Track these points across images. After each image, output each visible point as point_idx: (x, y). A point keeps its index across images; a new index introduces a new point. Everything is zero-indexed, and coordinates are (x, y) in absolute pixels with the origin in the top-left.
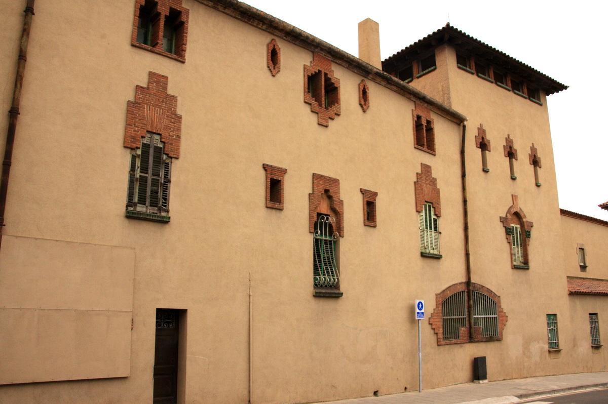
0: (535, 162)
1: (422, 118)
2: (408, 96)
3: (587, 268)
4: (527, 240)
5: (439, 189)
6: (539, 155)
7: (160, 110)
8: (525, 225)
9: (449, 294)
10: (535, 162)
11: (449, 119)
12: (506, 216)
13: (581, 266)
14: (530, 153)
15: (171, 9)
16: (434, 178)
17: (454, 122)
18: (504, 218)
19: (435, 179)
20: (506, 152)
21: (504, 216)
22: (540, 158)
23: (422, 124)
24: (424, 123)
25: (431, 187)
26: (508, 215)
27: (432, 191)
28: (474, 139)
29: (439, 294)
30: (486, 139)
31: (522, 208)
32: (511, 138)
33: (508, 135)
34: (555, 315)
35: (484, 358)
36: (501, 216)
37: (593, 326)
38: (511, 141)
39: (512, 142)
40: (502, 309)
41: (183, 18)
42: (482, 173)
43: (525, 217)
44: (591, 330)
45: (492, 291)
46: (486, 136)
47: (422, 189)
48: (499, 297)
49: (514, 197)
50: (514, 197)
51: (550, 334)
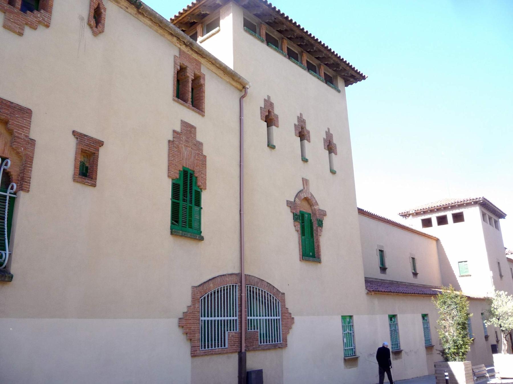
0: (330, 147)
1: (188, 69)
2: (170, 37)
3: (387, 271)
4: (319, 230)
5: (205, 157)
6: (335, 141)
7: (193, 151)
8: (317, 213)
9: (213, 287)
10: (330, 147)
12: (295, 201)
13: (413, 273)
14: (325, 137)
15: (195, 74)
16: (198, 142)
17: (233, 86)
18: (291, 202)
19: (201, 144)
20: (297, 132)
21: (293, 200)
22: (335, 145)
23: (188, 77)
24: (191, 76)
25: (193, 151)
26: (297, 199)
27: (195, 157)
28: (260, 109)
29: (196, 287)
30: (274, 112)
31: (313, 194)
32: (304, 117)
33: (301, 114)
34: (351, 317)
35: (262, 370)
36: (288, 199)
37: (425, 326)
38: (304, 122)
39: (305, 122)
40: (287, 309)
41: (202, 81)
42: (267, 149)
43: (317, 204)
44: (391, 333)
45: (274, 287)
46: (273, 110)
47: (179, 151)
48: (284, 294)
49: (305, 182)
50: (305, 182)
51: (345, 340)
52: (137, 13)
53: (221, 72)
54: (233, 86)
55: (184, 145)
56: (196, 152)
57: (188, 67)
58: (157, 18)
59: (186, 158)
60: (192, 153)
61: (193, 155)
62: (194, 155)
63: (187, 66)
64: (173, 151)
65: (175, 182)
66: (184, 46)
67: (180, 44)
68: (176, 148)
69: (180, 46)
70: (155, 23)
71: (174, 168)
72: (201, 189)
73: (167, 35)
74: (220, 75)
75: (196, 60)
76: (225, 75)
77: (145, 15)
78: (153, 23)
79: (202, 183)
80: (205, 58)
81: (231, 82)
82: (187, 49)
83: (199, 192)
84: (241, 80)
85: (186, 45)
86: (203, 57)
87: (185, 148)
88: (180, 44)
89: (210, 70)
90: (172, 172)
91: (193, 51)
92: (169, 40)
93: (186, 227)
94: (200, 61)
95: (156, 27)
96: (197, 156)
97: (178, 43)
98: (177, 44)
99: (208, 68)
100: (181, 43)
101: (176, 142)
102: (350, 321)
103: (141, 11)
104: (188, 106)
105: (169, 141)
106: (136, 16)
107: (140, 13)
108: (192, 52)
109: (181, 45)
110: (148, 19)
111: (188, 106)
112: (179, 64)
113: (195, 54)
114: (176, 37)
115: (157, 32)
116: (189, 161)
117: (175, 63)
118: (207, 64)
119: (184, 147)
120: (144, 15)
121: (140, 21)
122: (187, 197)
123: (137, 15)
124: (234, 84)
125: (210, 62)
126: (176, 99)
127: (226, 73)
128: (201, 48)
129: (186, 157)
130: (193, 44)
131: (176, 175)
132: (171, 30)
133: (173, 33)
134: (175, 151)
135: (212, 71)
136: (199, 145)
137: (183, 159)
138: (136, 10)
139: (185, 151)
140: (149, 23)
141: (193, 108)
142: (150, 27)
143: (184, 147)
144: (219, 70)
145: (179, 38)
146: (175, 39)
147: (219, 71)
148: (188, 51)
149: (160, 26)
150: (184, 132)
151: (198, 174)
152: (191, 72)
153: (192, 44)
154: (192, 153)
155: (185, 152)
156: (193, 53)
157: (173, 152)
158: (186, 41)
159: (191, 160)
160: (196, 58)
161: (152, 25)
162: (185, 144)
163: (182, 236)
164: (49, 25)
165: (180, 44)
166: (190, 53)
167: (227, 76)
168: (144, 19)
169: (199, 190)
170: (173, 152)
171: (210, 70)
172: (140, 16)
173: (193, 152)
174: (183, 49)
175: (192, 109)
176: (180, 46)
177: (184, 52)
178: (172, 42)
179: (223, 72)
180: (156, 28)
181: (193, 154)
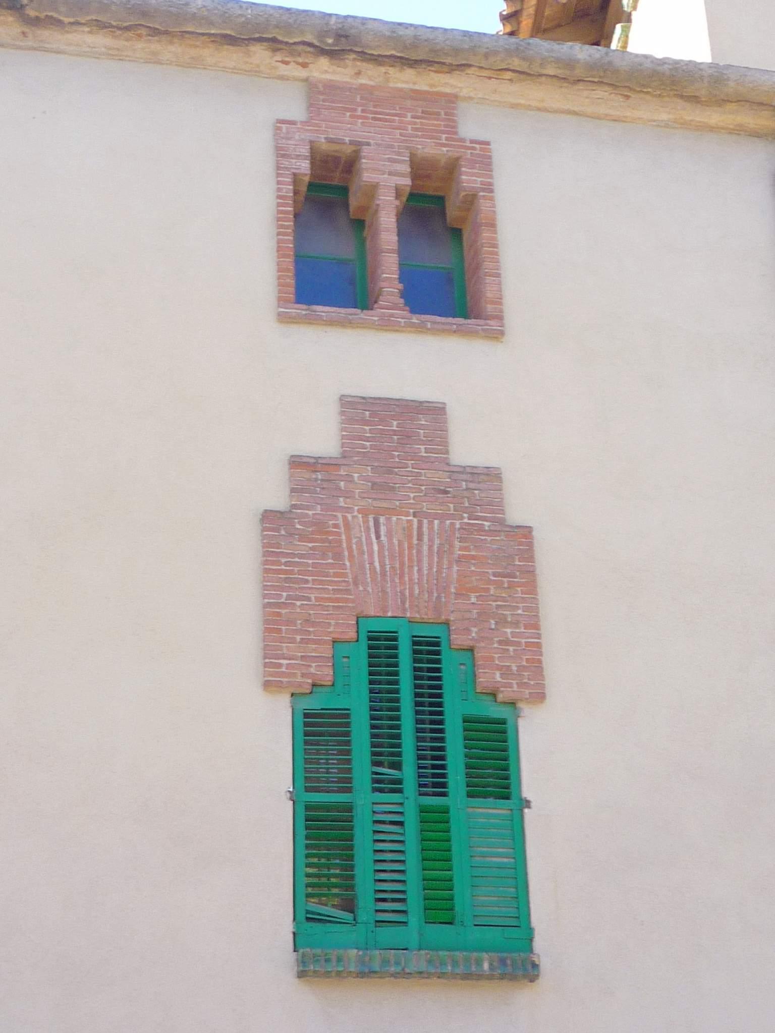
2: (231, 57)
7: (431, 523)
11: (664, 116)
17: (712, 129)
52: (26, 30)
53: (601, 93)
54: (712, 129)
55: (359, 511)
56: (452, 524)
57: (368, 144)
58: (113, 8)
59: (383, 573)
60: (420, 538)
61: (430, 547)
62: (437, 542)
63: (360, 144)
64: (283, 560)
65: (315, 704)
66: (324, 62)
67: (300, 60)
68: (303, 538)
69: (302, 73)
70: (127, 29)
71: (298, 638)
72: (513, 704)
73: (209, 53)
74: (602, 110)
75: (417, 95)
76: (628, 97)
77: (66, 20)
78: (119, 32)
79: (506, 672)
80: (470, 66)
81: (689, 118)
82: (346, 67)
83: (503, 722)
84: (732, 84)
85: (333, 54)
86: (453, 68)
87: (371, 524)
88: (298, 63)
89: (529, 108)
90: (285, 662)
91: (381, 64)
92: (235, 70)
93: (405, 923)
94: (448, 90)
95: (140, 45)
96: (457, 544)
97: (287, 63)
98: (283, 70)
99: (514, 106)
100: (299, 55)
101: (308, 508)
102: (499, 668)
103: (37, 14)
104: (382, 317)
105: (269, 518)
106: (30, 43)
107: (36, 22)
108: (383, 69)
109: (304, 65)
110: (87, 29)
111: (382, 317)
112: (305, 151)
113: (402, 70)
114: (260, 40)
115: (159, 63)
116: (402, 582)
117: (281, 153)
118: (495, 91)
119: (366, 522)
120: (56, 23)
121: (58, 52)
122: (397, 766)
123: (30, 36)
124: (714, 117)
125: (508, 75)
126: (301, 310)
127: (630, 89)
128: (410, 32)
129: (383, 566)
130: (353, 31)
131: (312, 670)
132: (211, 24)
133: (229, 32)
134: (301, 556)
135: (545, 110)
136: (472, 485)
137: (356, 583)
138: (11, 19)
139: (368, 538)
140: (101, 40)
141: (415, 319)
142: (115, 55)
143: (366, 522)
144: (581, 86)
145: (274, 40)
146: (260, 54)
147: (586, 93)
148: (358, 73)
149: (155, 32)
150: (364, 447)
151: (474, 630)
152: (390, 160)
153: (346, 37)
154: (420, 538)
155: (370, 544)
156: (391, 70)
157: (286, 564)
158: (309, 38)
159: (420, 570)
160: (417, 87)
161: (122, 43)
162: (363, 503)
163: (366, 973)
164: (504, 518)
165: (300, 60)
166: (370, 79)
167: (648, 97)
168: (70, 36)
169: (495, 711)
170: (286, 564)
171: (529, 108)
172: (47, 34)
173: (431, 529)
174: (328, 77)
175: (413, 325)
176: (302, 73)
177: (331, 88)
178: (255, 72)
179: (606, 88)
180: (141, 46)
181: (431, 540)
